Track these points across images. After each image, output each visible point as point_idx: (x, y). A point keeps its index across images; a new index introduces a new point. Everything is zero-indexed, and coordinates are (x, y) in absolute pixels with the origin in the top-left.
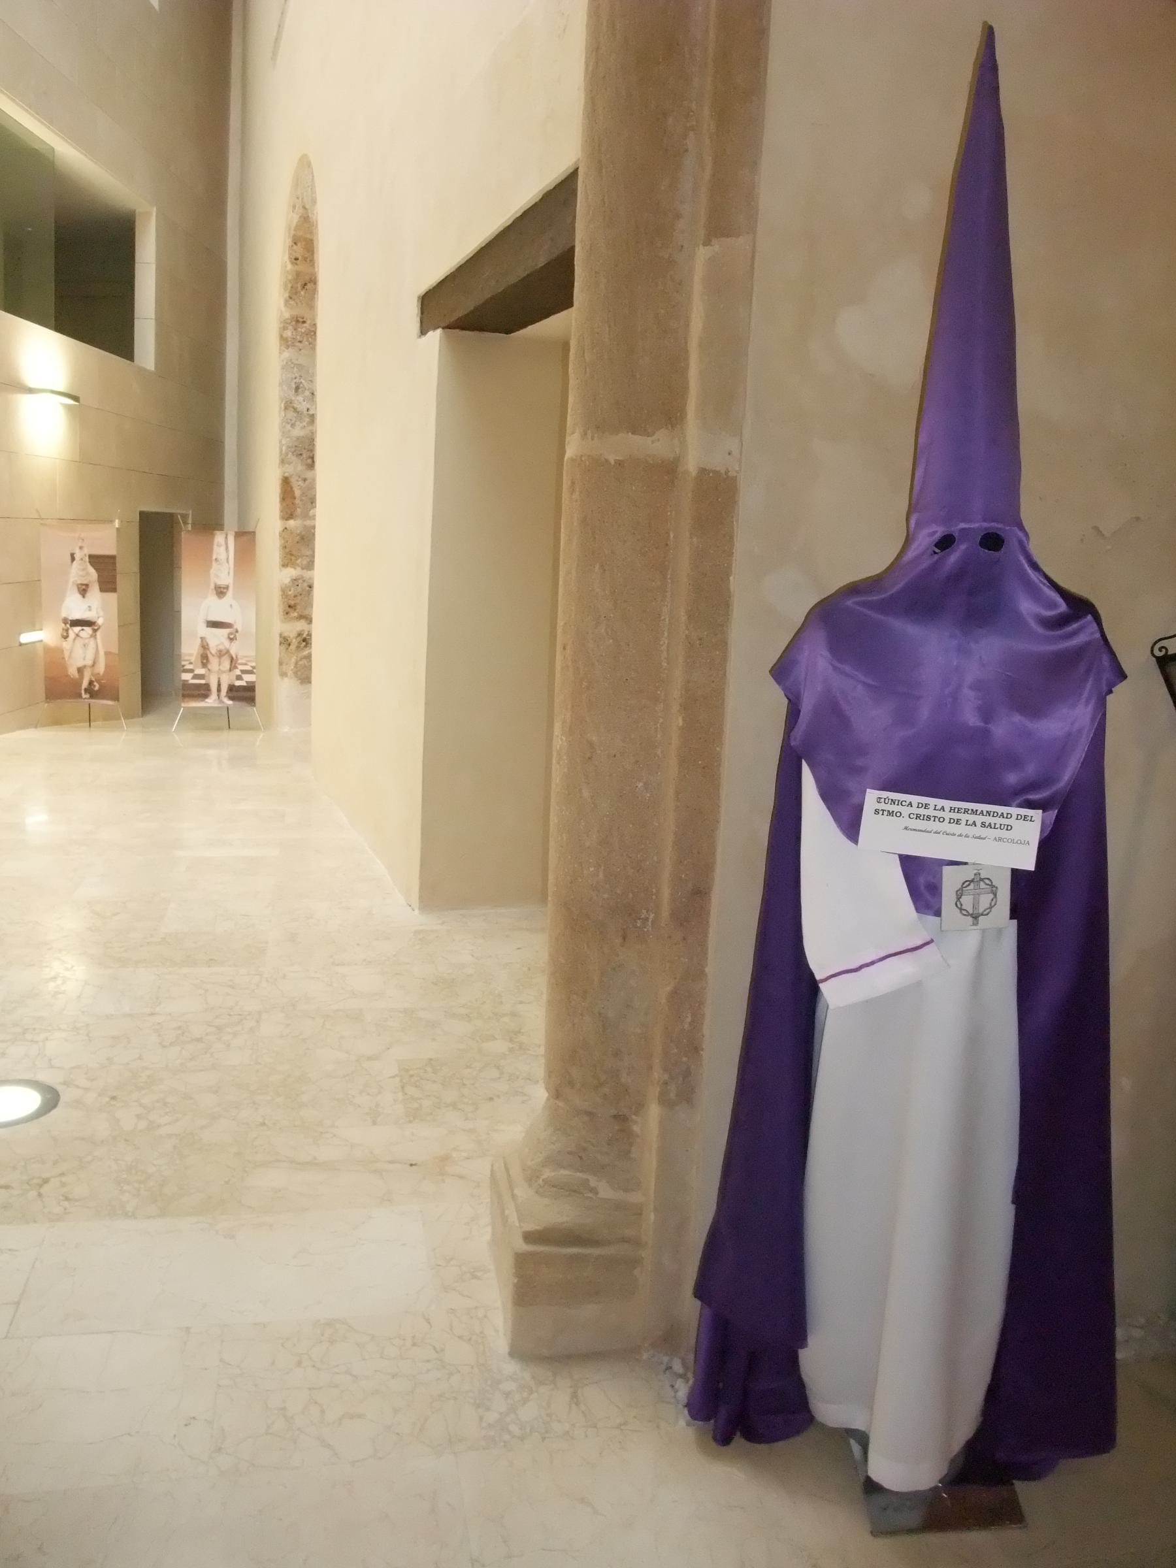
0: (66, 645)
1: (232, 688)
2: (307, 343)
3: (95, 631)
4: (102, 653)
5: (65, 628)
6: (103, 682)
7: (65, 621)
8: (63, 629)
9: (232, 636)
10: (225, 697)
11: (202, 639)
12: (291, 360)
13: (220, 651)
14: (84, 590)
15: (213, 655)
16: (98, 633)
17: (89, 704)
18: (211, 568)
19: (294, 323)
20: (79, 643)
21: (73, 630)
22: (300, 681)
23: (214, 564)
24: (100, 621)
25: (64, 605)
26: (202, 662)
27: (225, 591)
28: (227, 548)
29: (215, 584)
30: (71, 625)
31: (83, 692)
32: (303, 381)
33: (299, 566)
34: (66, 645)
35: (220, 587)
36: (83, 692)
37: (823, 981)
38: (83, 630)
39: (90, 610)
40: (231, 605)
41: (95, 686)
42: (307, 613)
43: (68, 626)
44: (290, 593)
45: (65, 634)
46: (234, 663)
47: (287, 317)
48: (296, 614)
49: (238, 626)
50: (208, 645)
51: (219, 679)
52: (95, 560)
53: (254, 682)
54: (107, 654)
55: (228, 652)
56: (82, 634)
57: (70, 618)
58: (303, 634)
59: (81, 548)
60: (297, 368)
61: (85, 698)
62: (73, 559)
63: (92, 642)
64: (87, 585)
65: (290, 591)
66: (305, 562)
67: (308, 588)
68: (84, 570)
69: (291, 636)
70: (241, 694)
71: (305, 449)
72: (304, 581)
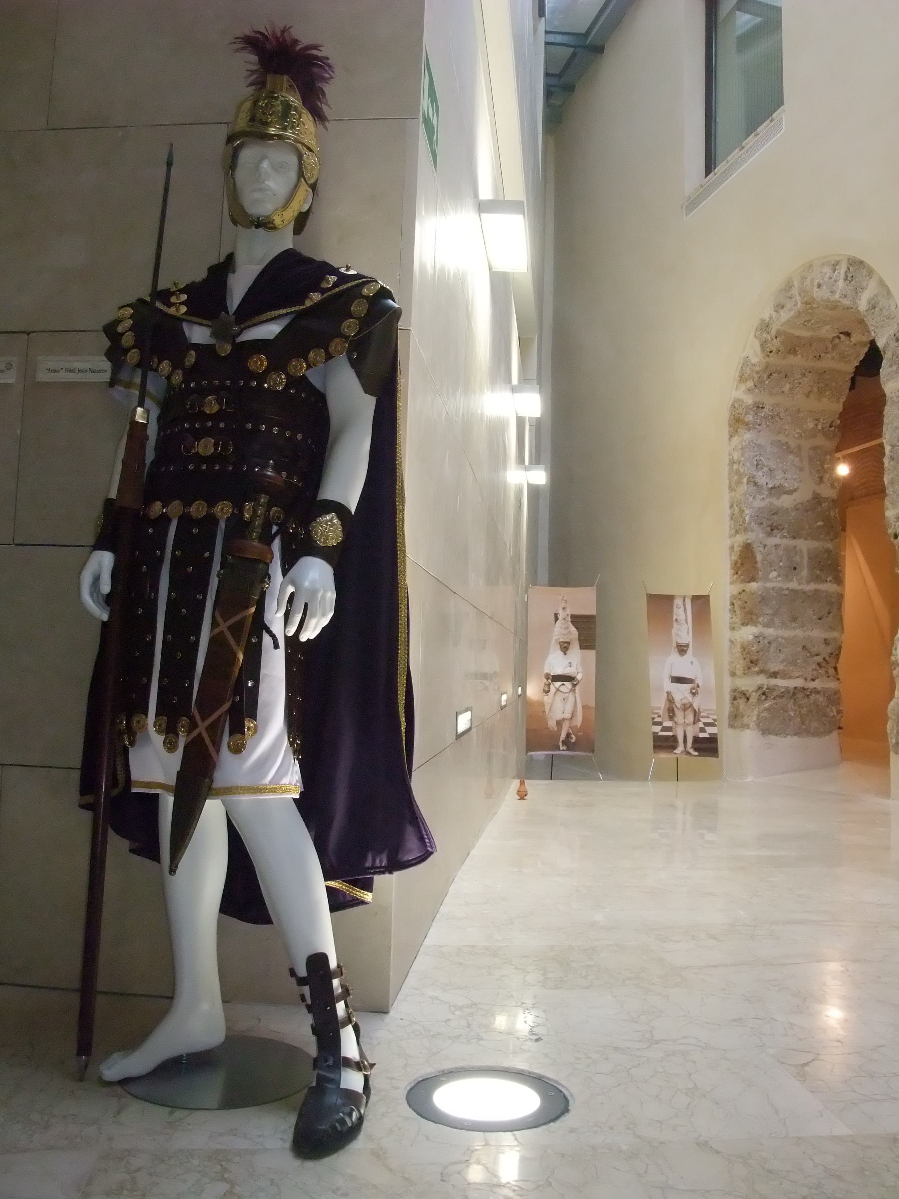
0: (547, 699)
1: (696, 740)
2: (765, 426)
3: (574, 686)
4: (580, 708)
5: (548, 683)
6: (579, 734)
7: (547, 677)
8: (545, 685)
9: (694, 691)
10: (691, 748)
11: (669, 693)
12: (752, 440)
13: (685, 705)
14: (565, 647)
15: (678, 709)
16: (577, 688)
17: (677, 758)
18: (673, 628)
19: (755, 408)
20: (559, 697)
21: (554, 685)
22: (761, 732)
23: (675, 625)
24: (579, 677)
25: (547, 662)
26: (669, 716)
27: (685, 649)
28: (685, 610)
29: (677, 643)
30: (553, 681)
31: (561, 744)
32: (763, 459)
33: (760, 624)
34: (547, 699)
35: (681, 646)
36: (561, 744)
37: (100, 992)
38: (563, 685)
39: (570, 666)
40: (692, 662)
41: (572, 738)
42: (768, 668)
43: (550, 681)
44: (754, 649)
45: (547, 689)
46: (697, 716)
47: (750, 404)
48: (757, 669)
49: (699, 681)
50: (673, 699)
51: (685, 731)
52: (576, 620)
53: (716, 734)
54: (585, 707)
55: (691, 706)
56: (563, 689)
57: (552, 674)
58: (762, 688)
59: (564, 609)
60: (757, 447)
61: (563, 750)
62: (557, 619)
63: (571, 695)
64: (569, 643)
65: (753, 647)
66: (766, 621)
67: (768, 645)
68: (567, 628)
69: (751, 690)
70: (705, 746)
71: (765, 518)
72: (765, 638)
